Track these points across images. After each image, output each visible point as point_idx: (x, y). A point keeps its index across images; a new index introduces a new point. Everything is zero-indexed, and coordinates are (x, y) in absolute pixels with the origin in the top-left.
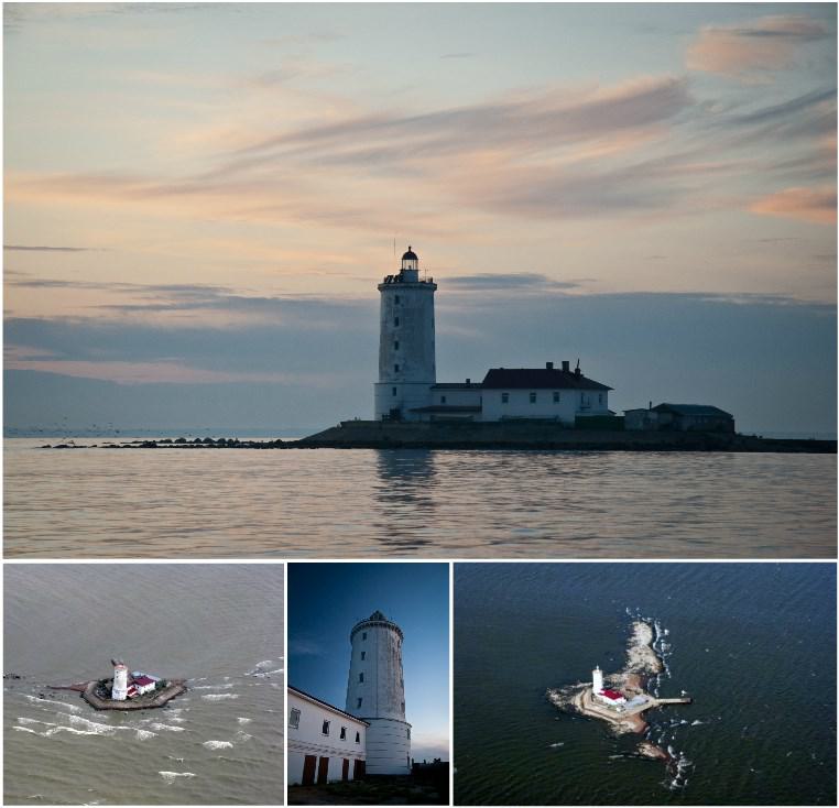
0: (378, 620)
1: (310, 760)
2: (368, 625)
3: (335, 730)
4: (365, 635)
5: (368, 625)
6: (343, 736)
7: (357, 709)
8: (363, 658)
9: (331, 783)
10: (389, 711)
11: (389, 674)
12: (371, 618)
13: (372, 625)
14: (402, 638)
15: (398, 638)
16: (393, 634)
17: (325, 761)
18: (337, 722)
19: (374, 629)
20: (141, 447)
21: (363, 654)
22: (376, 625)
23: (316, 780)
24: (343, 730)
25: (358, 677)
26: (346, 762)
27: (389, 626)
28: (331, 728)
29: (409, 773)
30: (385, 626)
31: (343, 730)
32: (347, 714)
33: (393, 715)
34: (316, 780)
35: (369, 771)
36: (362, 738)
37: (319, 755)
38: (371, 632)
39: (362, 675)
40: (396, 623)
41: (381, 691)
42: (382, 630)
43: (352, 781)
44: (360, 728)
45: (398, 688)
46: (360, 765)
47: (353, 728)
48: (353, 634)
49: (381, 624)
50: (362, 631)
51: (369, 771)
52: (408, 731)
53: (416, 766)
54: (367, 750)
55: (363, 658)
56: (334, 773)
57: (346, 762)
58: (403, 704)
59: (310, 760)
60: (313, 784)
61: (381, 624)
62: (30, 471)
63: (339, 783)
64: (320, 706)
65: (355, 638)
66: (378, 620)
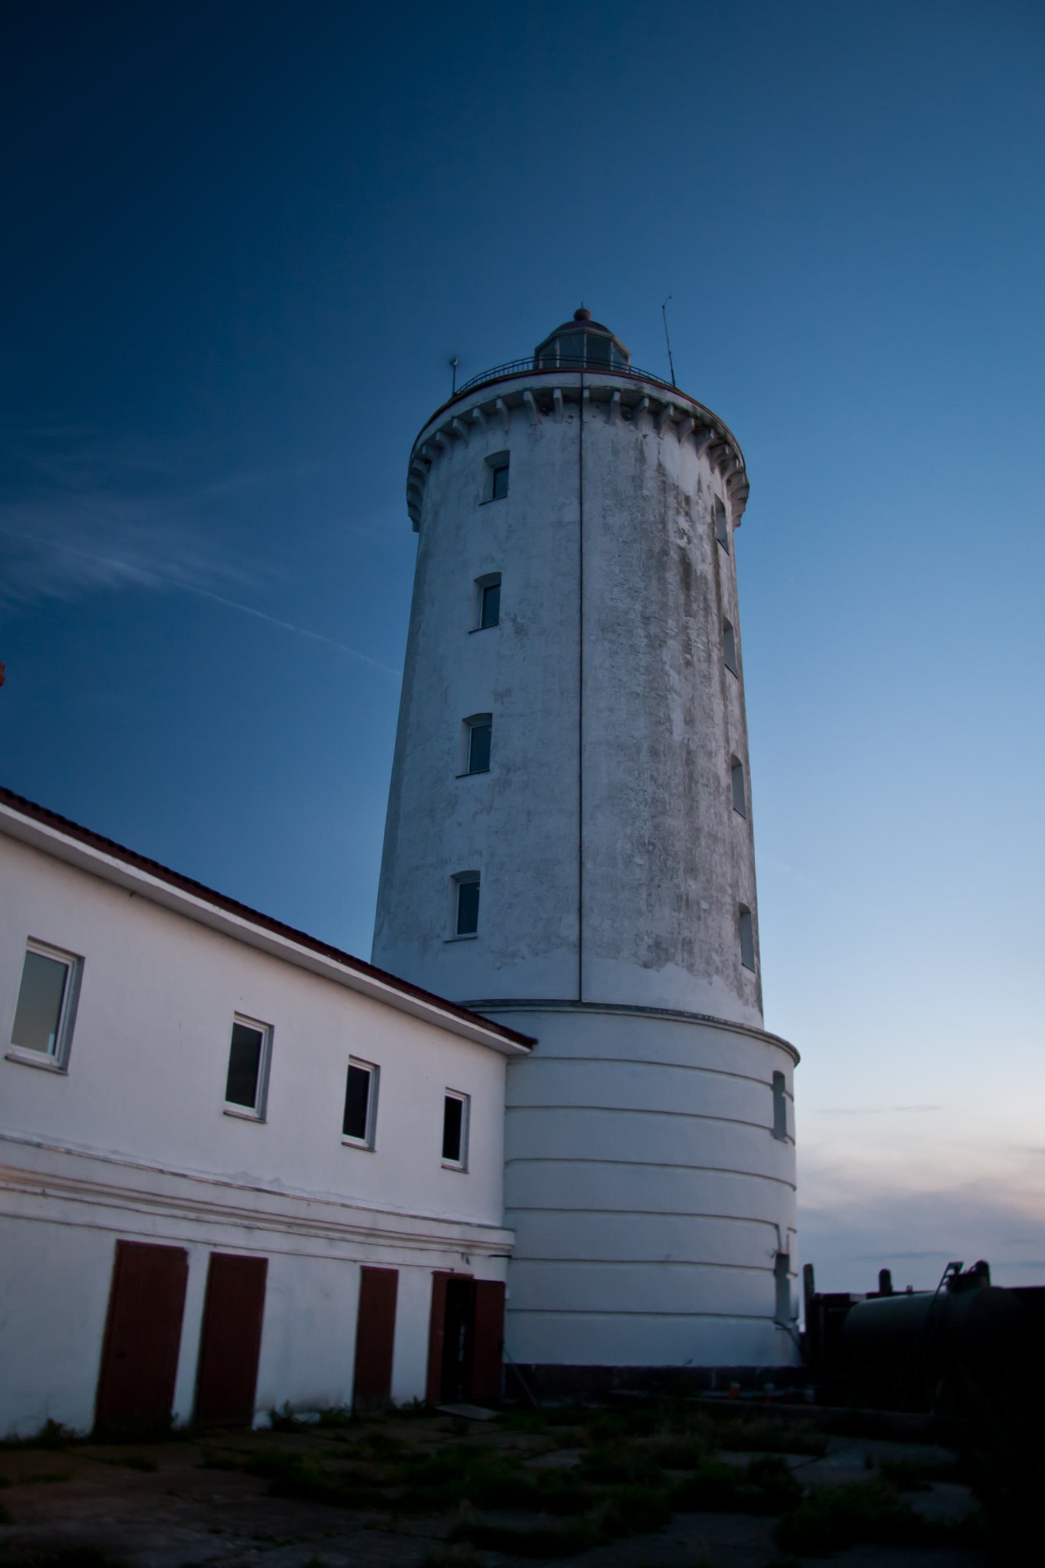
0: (582, 371)
1: (145, 1277)
2: (515, 404)
3: (303, 1086)
4: (499, 467)
5: (515, 404)
6: (357, 1118)
7: (448, 945)
8: (489, 617)
9: (284, 1423)
10: (659, 953)
11: (661, 722)
12: (543, 351)
13: (546, 403)
14: (741, 492)
15: (717, 485)
16: (688, 466)
17: (240, 1284)
18: (319, 1031)
19: (556, 430)
20: (738, 676)
21: (489, 588)
22: (574, 399)
23: (183, 1402)
24: (360, 1085)
25: (459, 738)
26: (378, 1289)
27: (658, 410)
28: (280, 1073)
29: (781, 1355)
30: (631, 408)
31: (360, 1085)
32: (388, 981)
33: (674, 986)
34: (183, 1402)
35: (527, 1343)
36: (481, 1129)
37: (201, 1242)
38: (540, 447)
39: (480, 730)
40: (701, 389)
41: (601, 829)
42: (604, 432)
43: (415, 1411)
44: (466, 1067)
45: (712, 810)
46: (466, 1306)
47: (424, 1065)
48: (424, 461)
49: (602, 400)
50: (472, 455)
51: (527, 1343)
52: (779, 1083)
53: (827, 1308)
54: (512, 1210)
55: (489, 617)
56: (304, 1356)
57: (378, 1289)
58: (746, 917)
59: (145, 1277)
60: (156, 1423)
61: (602, 400)
62: (101, 1154)
63: (331, 1419)
64: (135, 893)
65: (432, 493)
66: (582, 371)
